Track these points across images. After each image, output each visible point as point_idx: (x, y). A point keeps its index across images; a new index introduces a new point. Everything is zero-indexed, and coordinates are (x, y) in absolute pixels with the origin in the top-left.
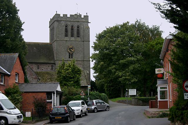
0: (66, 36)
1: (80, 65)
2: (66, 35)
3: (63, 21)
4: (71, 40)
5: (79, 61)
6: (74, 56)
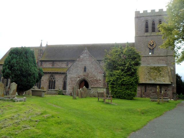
0: (146, 32)
1: (163, 61)
2: (147, 31)
3: (143, 17)
4: (152, 35)
5: (161, 57)
6: (156, 51)
